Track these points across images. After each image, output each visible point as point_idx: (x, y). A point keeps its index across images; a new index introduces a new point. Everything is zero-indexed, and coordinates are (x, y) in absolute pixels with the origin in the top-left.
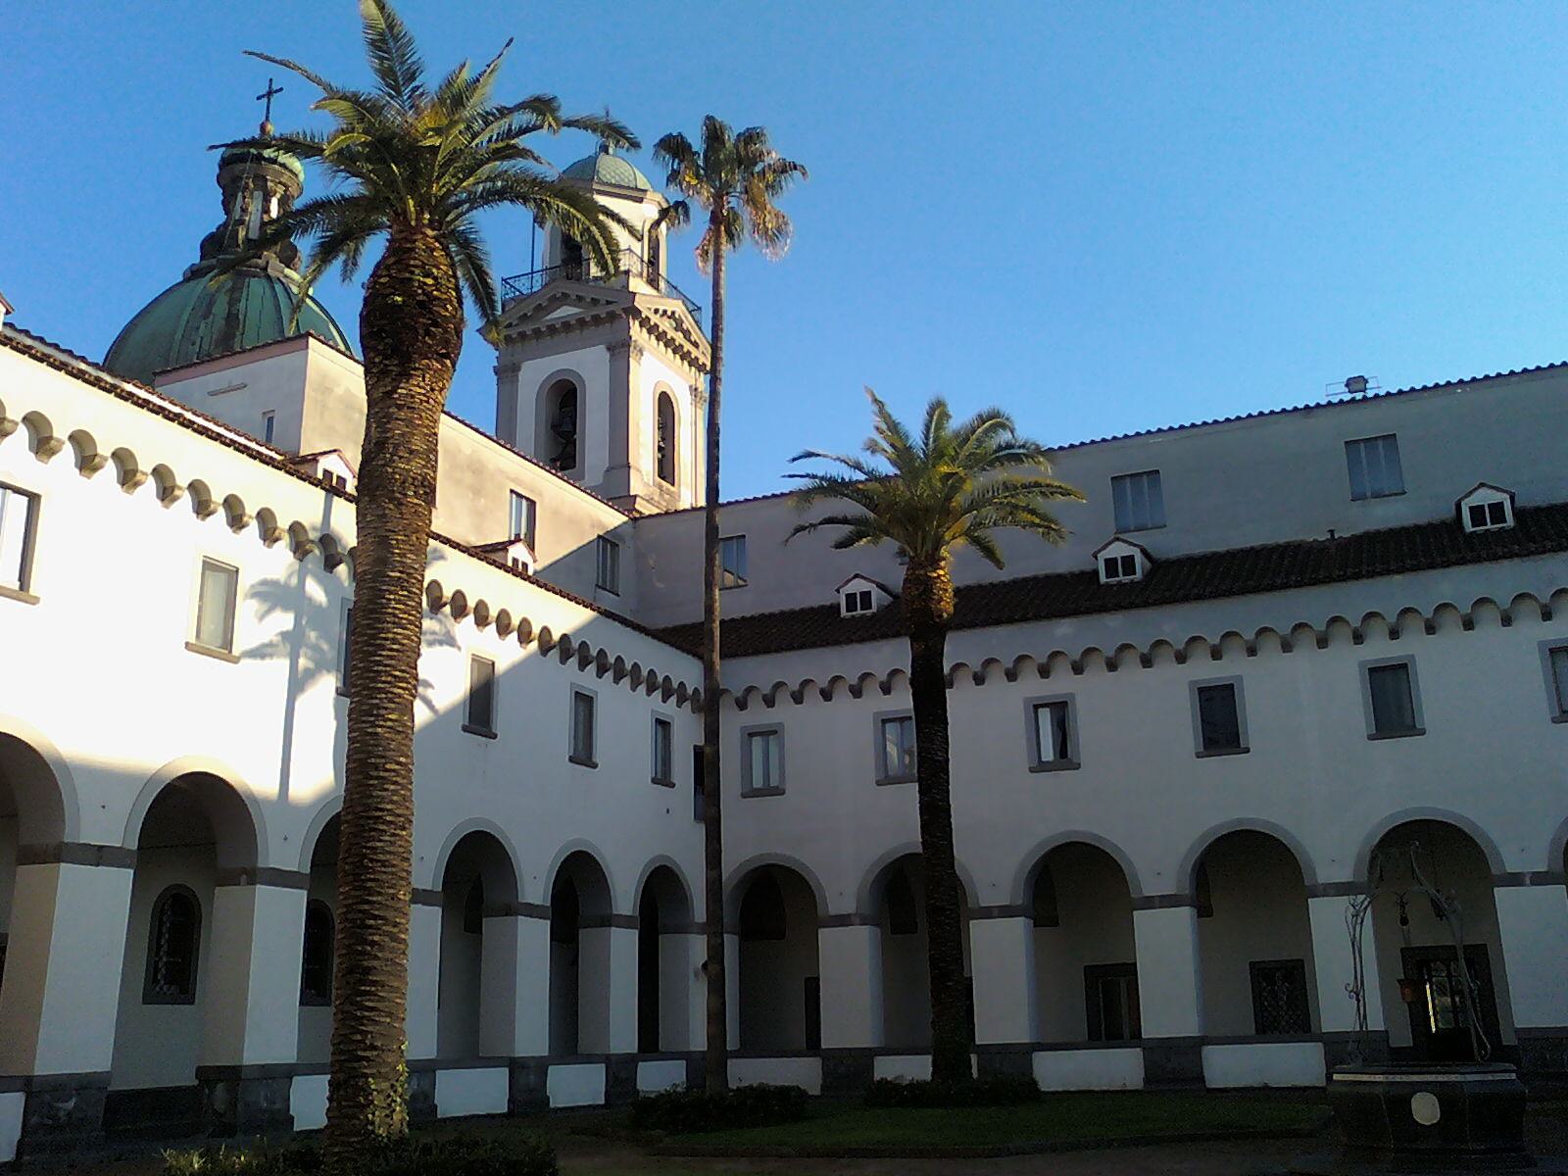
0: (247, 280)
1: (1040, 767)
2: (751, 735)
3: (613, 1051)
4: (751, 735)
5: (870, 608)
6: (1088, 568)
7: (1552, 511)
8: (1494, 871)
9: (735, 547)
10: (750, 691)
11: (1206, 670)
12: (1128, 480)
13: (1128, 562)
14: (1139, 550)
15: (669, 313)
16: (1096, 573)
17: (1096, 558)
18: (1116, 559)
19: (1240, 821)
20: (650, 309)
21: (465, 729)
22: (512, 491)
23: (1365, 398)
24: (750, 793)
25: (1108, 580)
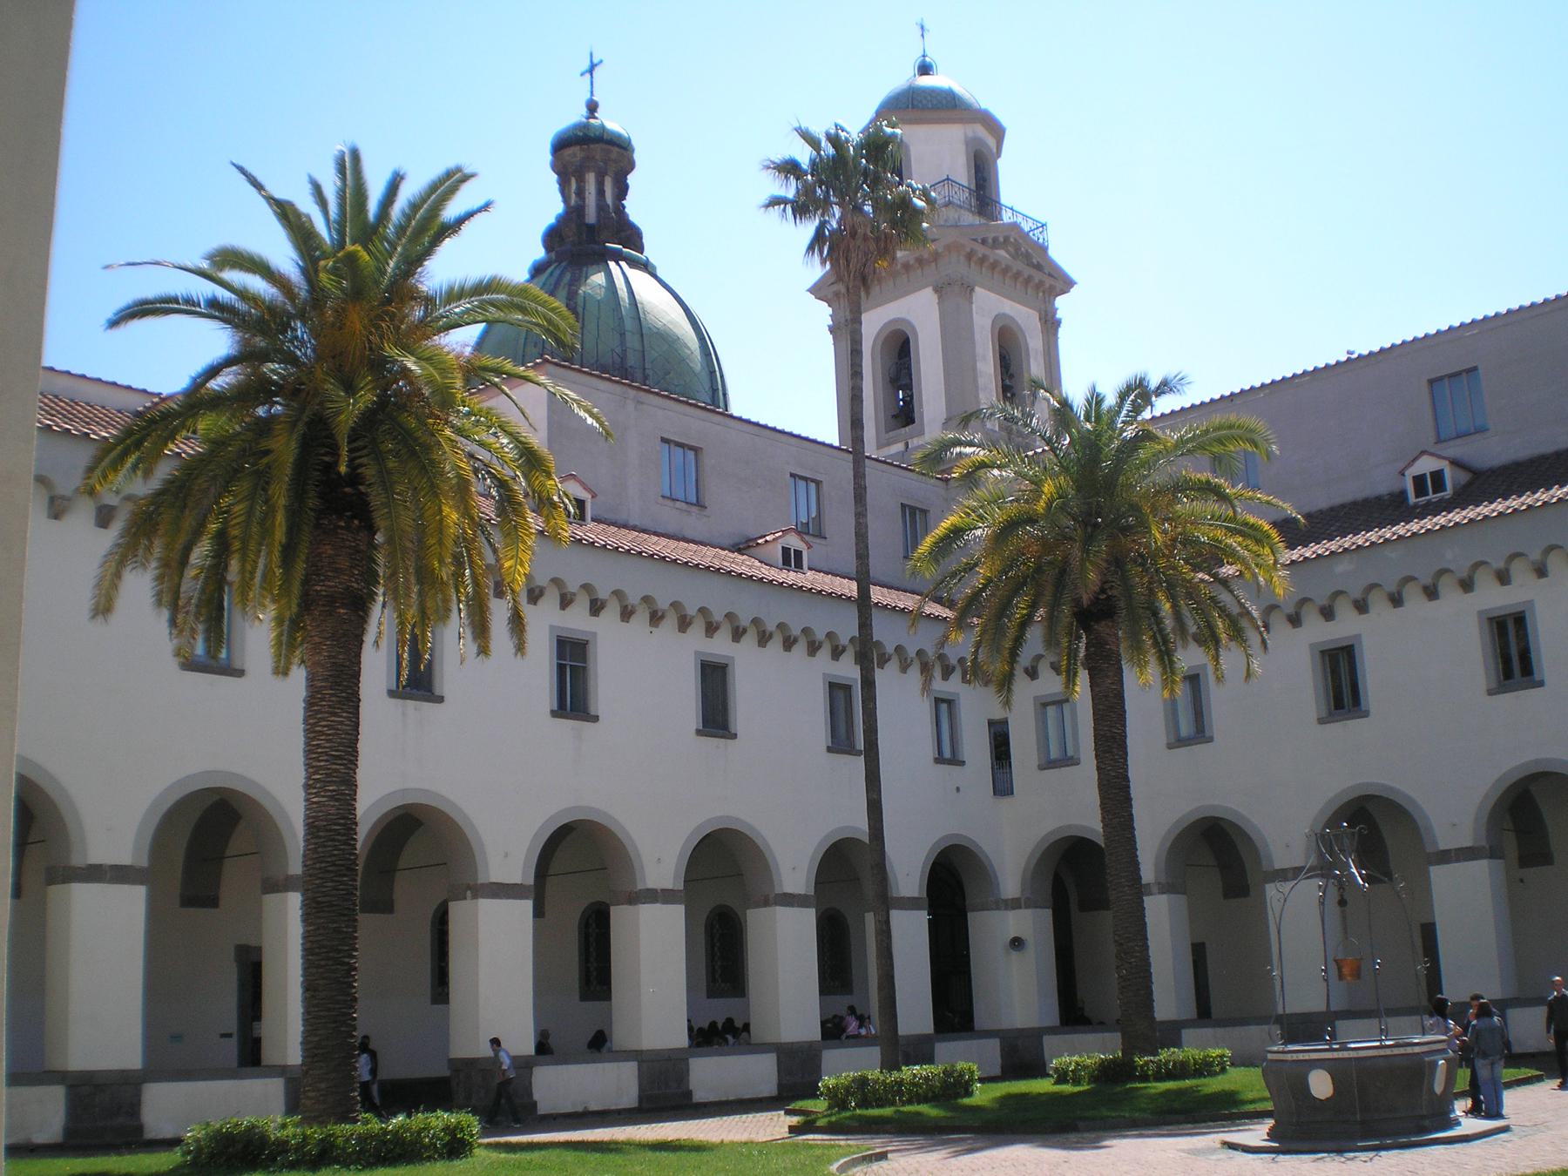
0: (585, 269)
1: (1177, 742)
2: (1045, 705)
3: (71, 1068)
4: (1045, 705)
5: (1445, 490)
6: (1396, 488)
7: (1558, 455)
8: (1429, 849)
9: (1465, 382)
10: (1552, 549)
11: (1493, 597)
12: (1464, 374)
13: (1438, 477)
14: (1447, 462)
15: (1001, 239)
16: (1403, 493)
17: (1403, 475)
18: (1425, 474)
19: (1537, 762)
20: (975, 240)
21: (699, 732)
22: (792, 475)
23: (766, 541)
24: (1048, 764)
25: (1417, 500)
